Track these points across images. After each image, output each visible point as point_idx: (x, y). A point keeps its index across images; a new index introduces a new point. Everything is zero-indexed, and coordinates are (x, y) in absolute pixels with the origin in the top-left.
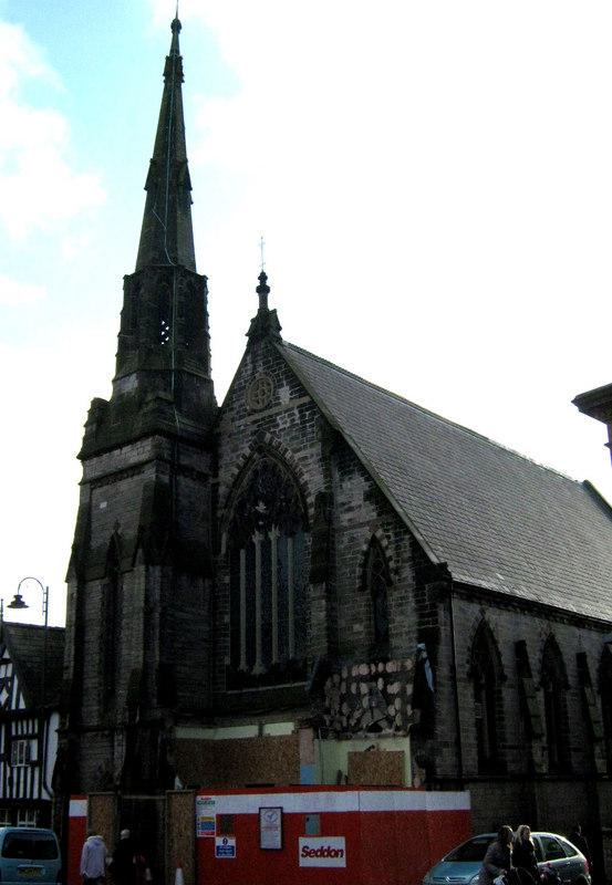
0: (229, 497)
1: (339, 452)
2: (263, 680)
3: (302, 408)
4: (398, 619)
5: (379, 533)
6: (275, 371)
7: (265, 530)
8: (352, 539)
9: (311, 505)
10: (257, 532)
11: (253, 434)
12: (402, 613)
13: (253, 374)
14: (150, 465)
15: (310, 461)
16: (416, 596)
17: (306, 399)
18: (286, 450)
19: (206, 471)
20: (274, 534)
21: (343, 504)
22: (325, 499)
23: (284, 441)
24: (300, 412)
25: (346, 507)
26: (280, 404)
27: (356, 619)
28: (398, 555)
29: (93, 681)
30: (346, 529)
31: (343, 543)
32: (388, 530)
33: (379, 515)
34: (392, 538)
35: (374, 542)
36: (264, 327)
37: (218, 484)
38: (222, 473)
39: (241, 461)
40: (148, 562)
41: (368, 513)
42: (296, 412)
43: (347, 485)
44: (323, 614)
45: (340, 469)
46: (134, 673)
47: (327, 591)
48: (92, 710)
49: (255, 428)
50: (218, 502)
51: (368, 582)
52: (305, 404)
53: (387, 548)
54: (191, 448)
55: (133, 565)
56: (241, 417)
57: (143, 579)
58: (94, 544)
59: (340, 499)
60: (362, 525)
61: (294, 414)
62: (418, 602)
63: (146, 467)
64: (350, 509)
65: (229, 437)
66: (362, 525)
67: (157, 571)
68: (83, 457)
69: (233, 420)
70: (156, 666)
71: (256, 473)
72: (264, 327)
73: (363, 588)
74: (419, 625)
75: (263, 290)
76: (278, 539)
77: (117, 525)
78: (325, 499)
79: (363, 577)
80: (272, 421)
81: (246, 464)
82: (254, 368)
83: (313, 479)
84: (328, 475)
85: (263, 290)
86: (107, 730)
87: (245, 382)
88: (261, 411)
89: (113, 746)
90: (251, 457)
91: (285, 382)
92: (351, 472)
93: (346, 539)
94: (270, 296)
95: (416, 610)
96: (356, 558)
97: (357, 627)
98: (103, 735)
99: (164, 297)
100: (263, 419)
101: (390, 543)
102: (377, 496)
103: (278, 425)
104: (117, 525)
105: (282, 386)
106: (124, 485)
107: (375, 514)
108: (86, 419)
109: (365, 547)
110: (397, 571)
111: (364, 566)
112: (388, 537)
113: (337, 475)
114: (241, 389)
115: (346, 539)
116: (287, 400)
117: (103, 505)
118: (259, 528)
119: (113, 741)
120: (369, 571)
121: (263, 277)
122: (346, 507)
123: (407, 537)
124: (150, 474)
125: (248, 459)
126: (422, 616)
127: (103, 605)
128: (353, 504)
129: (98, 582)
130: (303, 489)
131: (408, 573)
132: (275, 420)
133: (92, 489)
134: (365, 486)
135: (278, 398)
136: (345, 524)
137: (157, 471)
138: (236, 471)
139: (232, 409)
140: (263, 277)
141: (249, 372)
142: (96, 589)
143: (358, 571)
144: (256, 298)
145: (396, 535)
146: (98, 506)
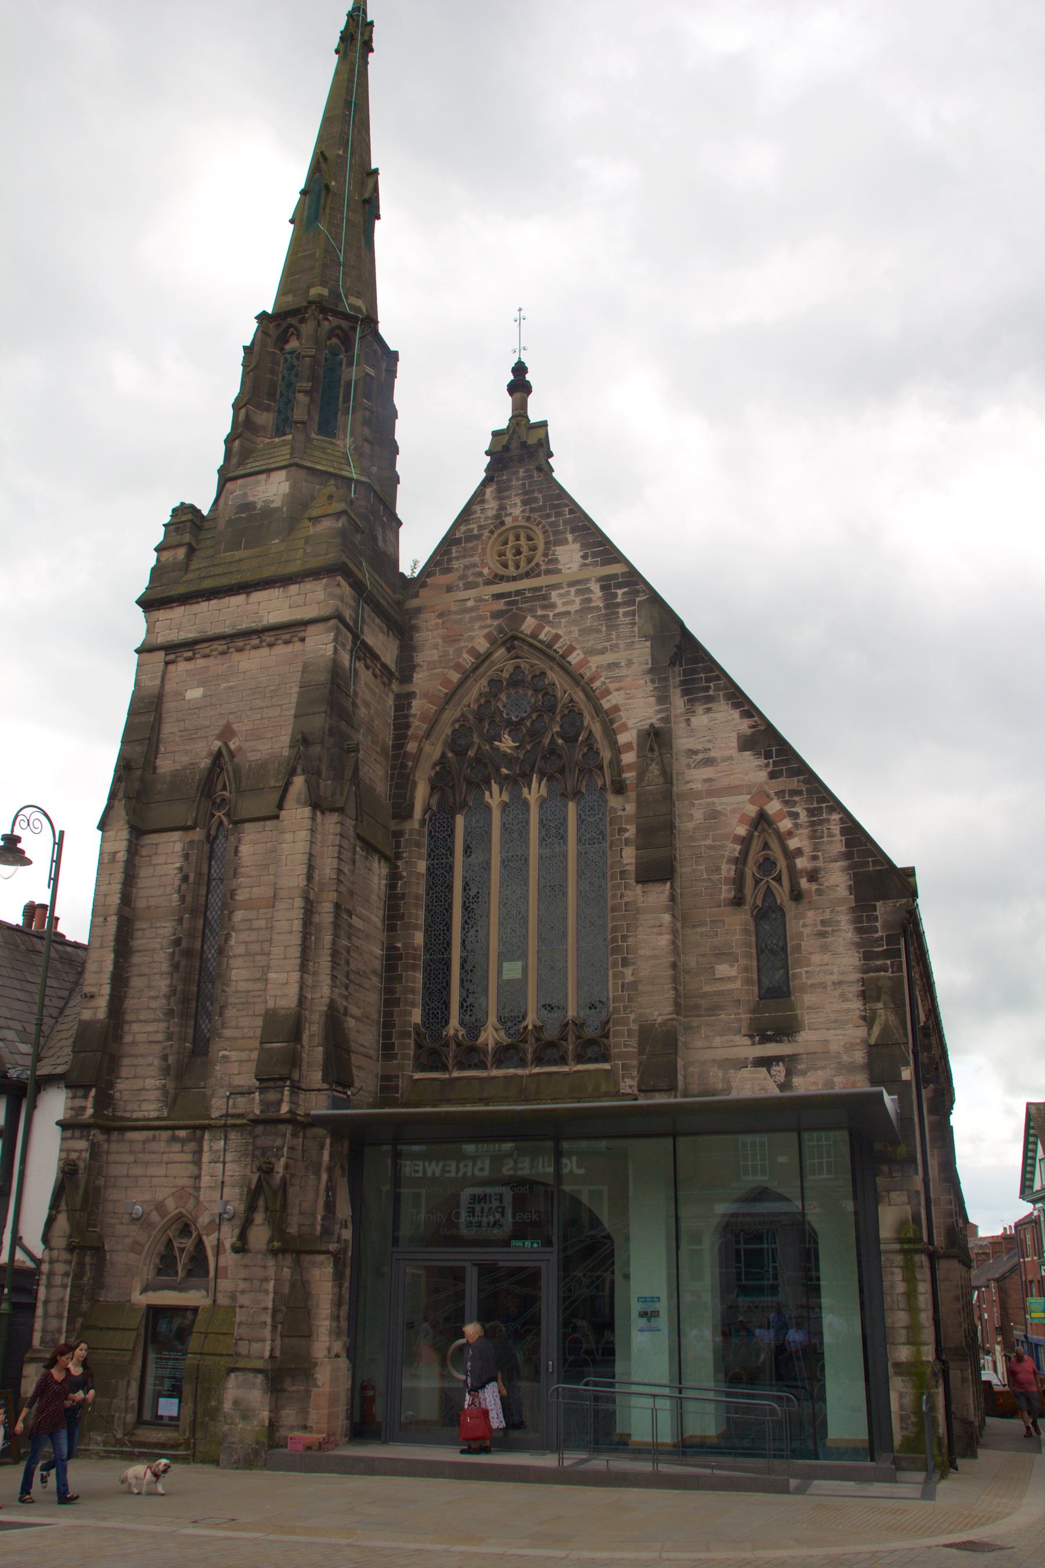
0: (434, 723)
1: (686, 664)
2: (505, 1054)
3: (607, 584)
4: (816, 958)
5: (774, 807)
6: (549, 516)
7: (517, 781)
8: (713, 815)
9: (628, 746)
10: (495, 787)
11: (495, 615)
12: (824, 949)
13: (498, 516)
14: (321, 627)
15: (624, 672)
16: (857, 920)
17: (617, 569)
18: (571, 649)
19: (393, 667)
20: (535, 792)
21: (693, 752)
22: (657, 739)
23: (565, 633)
24: (603, 588)
25: (700, 756)
26: (558, 571)
27: (723, 954)
28: (816, 847)
29: (152, 1027)
30: (697, 795)
31: (691, 819)
32: (794, 804)
33: (773, 775)
34: (803, 817)
35: (762, 820)
36: (520, 451)
37: (411, 695)
38: (419, 677)
39: (467, 660)
40: (317, 804)
41: (751, 769)
42: (595, 587)
43: (701, 720)
44: (664, 940)
45: (685, 692)
46: (271, 1018)
47: (673, 898)
48: (142, 1088)
49: (500, 605)
50: (408, 726)
51: (748, 890)
52: (614, 576)
53: (790, 834)
54: (377, 620)
55: (280, 806)
56: (469, 586)
57: (304, 834)
58: (166, 765)
59: (683, 741)
60: (732, 790)
61: (589, 590)
62: (859, 931)
63: (311, 629)
64: (709, 762)
65: (441, 615)
66: (732, 790)
67: (331, 823)
68: (148, 603)
69: (449, 589)
70: (321, 1007)
71: (495, 683)
72: (520, 451)
73: (738, 901)
74: (866, 971)
75: (519, 385)
76: (543, 802)
77: (227, 733)
78: (657, 739)
79: (738, 882)
80: (541, 596)
81: (476, 668)
82: (502, 508)
83: (635, 706)
84: (663, 698)
85: (519, 385)
86: (188, 1119)
87: (480, 528)
88: (514, 579)
89: (198, 1163)
90: (489, 655)
91: (570, 537)
92: (709, 699)
93: (698, 814)
94: (531, 400)
95: (858, 945)
96: (723, 847)
97: (723, 969)
98: (174, 1139)
99: (318, 359)
100: (518, 593)
101: (797, 826)
102: (767, 743)
103: (553, 606)
104: (227, 733)
105: (564, 542)
106: (251, 662)
107: (763, 775)
108: (158, 536)
109: (742, 831)
110: (813, 876)
111: (740, 861)
112: (795, 816)
113: (678, 702)
114: (470, 538)
115: (698, 814)
116: (575, 566)
117: (195, 693)
118: (503, 781)
119: (199, 1152)
120: (750, 869)
121: (520, 369)
122: (700, 756)
123: (835, 817)
124: (321, 644)
125: (482, 659)
126: (867, 956)
127: (185, 879)
128: (712, 754)
129: (176, 835)
130: (609, 720)
131: (837, 879)
132: (545, 597)
133: (167, 663)
134: (736, 724)
135: (555, 561)
136: (697, 786)
137: (336, 640)
138: (455, 677)
139: (449, 570)
140: (520, 369)
141: (490, 513)
142: (169, 855)
143: (728, 870)
144: (507, 401)
145: (811, 812)
146: (180, 695)
